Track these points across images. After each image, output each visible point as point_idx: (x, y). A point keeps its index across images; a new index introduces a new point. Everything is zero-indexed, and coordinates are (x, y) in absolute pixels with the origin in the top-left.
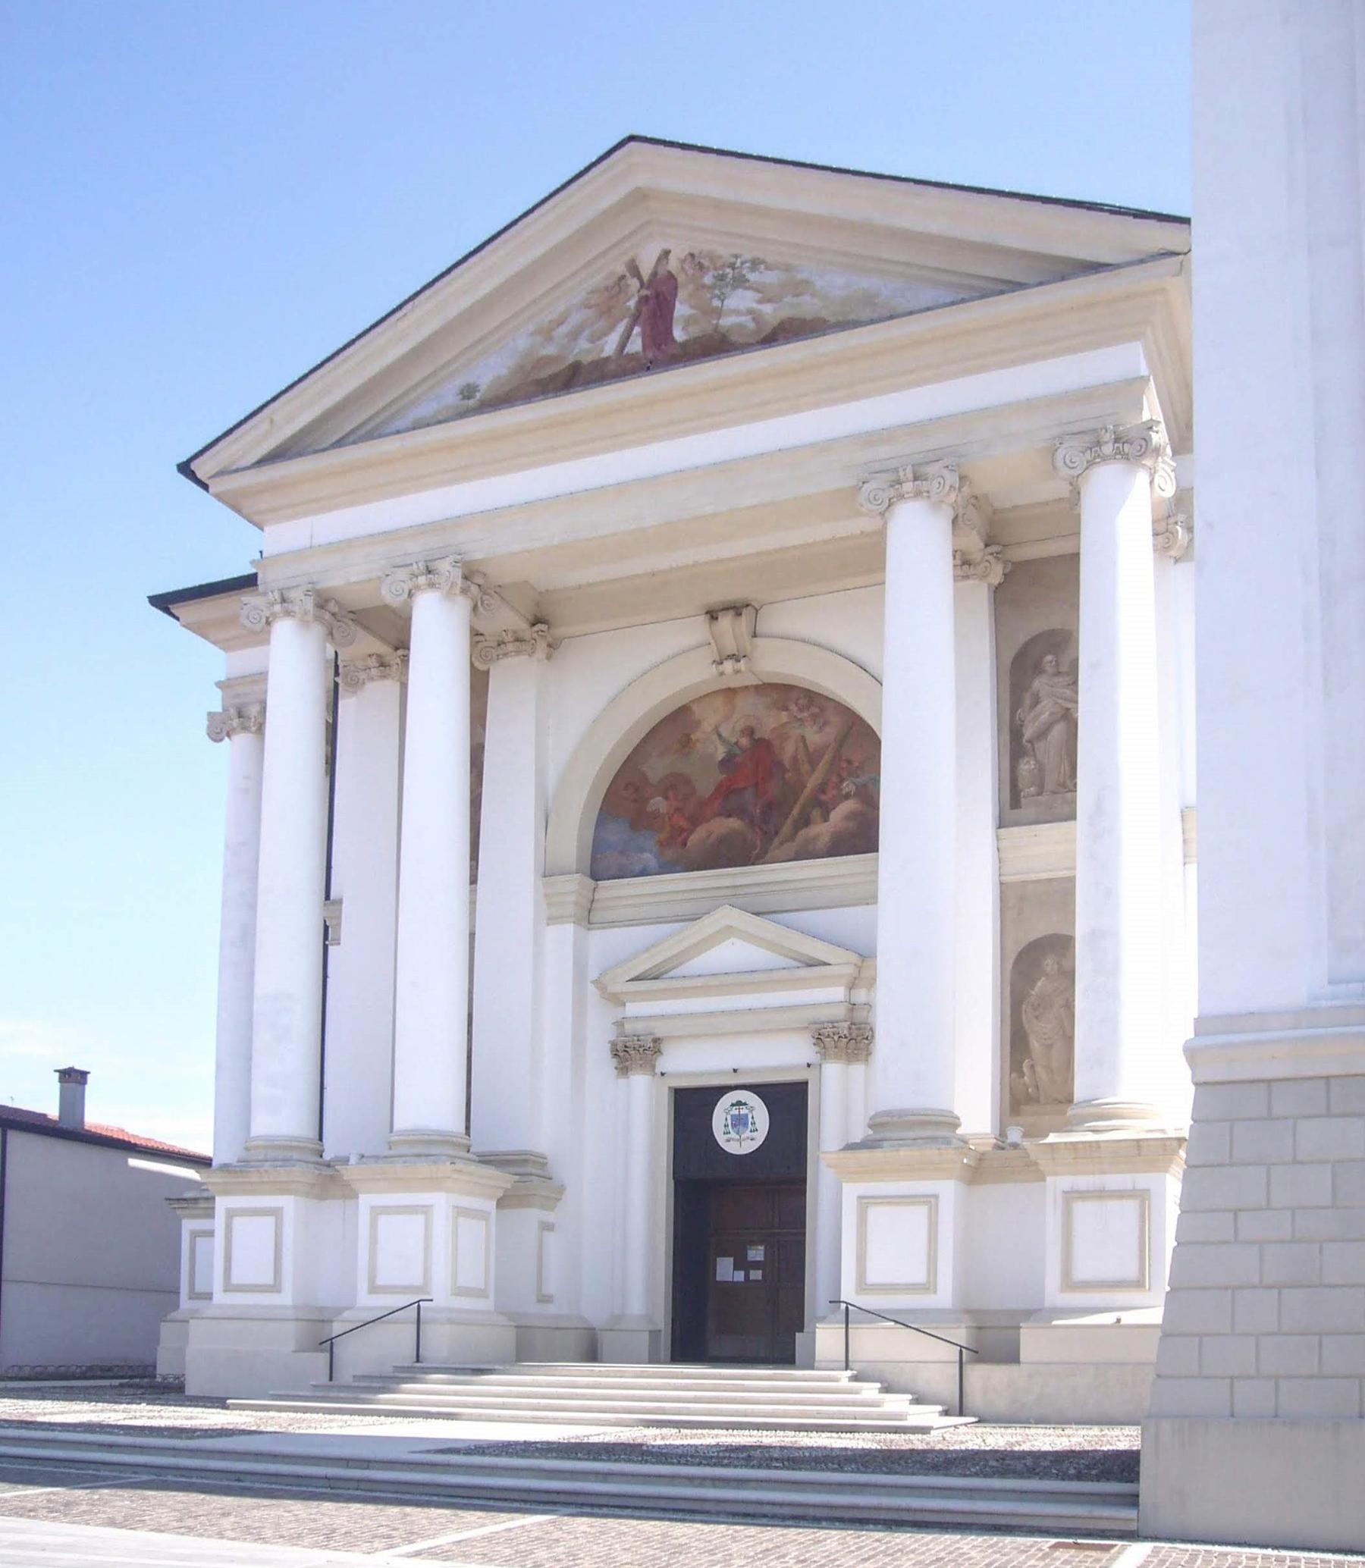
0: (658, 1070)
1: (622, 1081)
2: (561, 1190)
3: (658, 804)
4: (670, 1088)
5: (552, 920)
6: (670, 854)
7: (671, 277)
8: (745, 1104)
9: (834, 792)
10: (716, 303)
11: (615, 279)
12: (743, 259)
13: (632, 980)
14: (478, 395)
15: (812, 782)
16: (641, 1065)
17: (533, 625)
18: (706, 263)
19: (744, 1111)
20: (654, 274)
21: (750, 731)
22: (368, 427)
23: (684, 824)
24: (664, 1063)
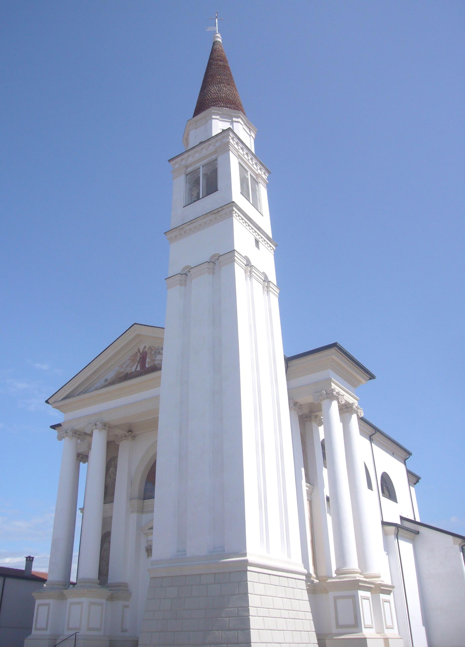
5: (132, 512)
7: (146, 352)
10: (154, 358)
11: (135, 353)
12: (160, 348)
13: (149, 529)
14: (108, 381)
17: (128, 432)
18: (153, 349)
20: (143, 352)
22: (84, 391)
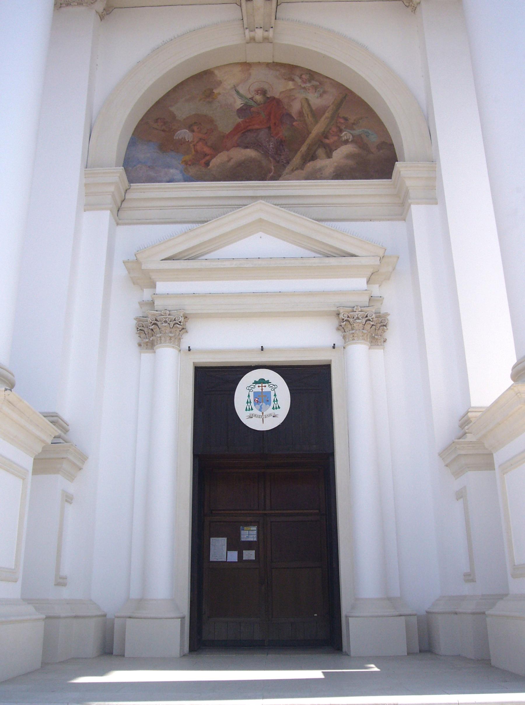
0: (184, 346)
1: (147, 356)
2: (84, 458)
3: (184, 134)
4: (331, 360)
6: (193, 170)
8: (268, 382)
9: (336, 138)
15: (316, 130)
16: (171, 338)
19: (267, 389)
21: (263, 92)
23: (206, 150)
24: (187, 340)
